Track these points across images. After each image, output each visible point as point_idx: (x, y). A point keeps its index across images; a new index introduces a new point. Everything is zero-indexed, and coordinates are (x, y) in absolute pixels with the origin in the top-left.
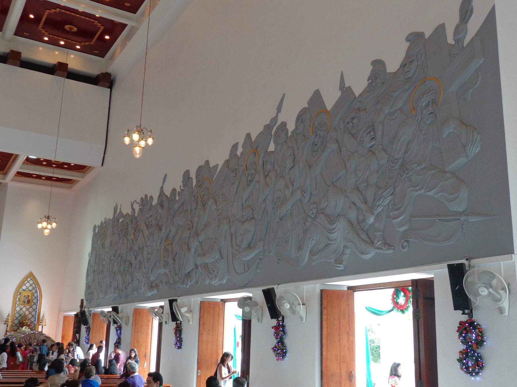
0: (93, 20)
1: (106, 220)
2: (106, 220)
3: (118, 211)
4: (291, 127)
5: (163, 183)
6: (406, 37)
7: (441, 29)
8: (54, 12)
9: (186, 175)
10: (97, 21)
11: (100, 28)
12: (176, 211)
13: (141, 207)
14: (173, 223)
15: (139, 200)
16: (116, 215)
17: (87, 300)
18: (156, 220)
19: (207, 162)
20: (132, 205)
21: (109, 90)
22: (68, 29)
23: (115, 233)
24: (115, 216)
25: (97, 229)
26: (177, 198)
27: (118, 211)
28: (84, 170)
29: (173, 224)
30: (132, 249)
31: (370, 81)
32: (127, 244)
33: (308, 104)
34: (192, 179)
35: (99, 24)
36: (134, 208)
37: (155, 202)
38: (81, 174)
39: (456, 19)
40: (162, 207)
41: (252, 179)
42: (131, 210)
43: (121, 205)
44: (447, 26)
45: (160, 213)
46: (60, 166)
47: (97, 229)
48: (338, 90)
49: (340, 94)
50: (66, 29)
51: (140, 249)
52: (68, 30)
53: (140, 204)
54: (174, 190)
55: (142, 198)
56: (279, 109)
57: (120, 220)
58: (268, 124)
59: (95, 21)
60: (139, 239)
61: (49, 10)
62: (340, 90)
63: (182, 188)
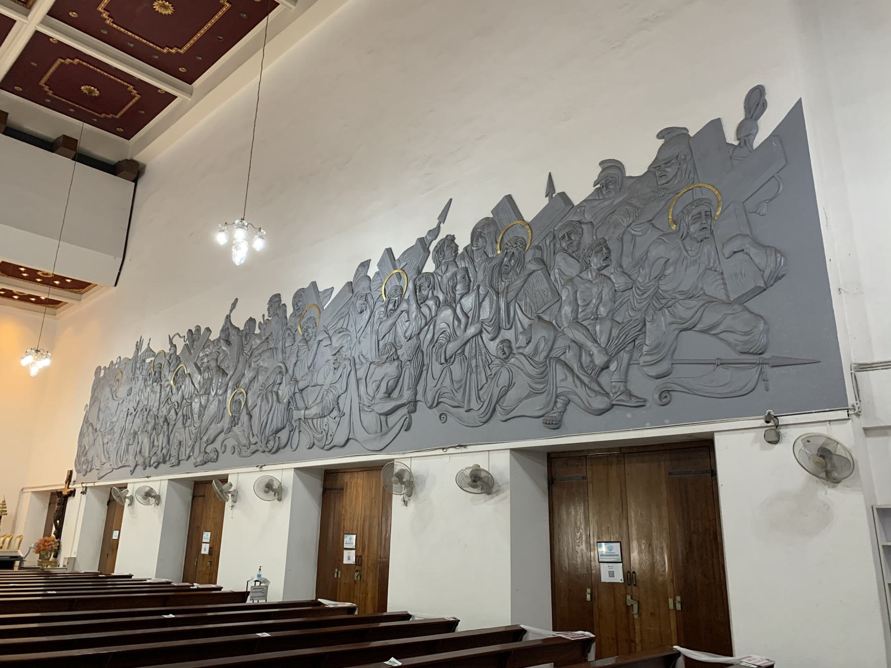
0: (126, 84)
1: (120, 360)
2: (120, 360)
3: (144, 347)
4: (463, 241)
5: (231, 311)
6: (657, 133)
7: (716, 125)
8: (70, 63)
9: (275, 301)
10: (131, 87)
11: (134, 97)
12: (254, 349)
13: (187, 342)
14: (251, 364)
15: (184, 333)
16: (139, 354)
17: (78, 472)
18: (217, 360)
19: (314, 284)
20: (171, 340)
21: (133, 184)
22: (85, 91)
23: (137, 377)
24: (138, 353)
25: (103, 371)
26: (257, 331)
27: (144, 347)
28: (84, 290)
29: (250, 367)
30: (169, 399)
31: (598, 186)
32: (161, 392)
33: (492, 213)
34: (286, 306)
35: (135, 92)
36: (174, 343)
37: (215, 335)
38: (78, 296)
39: (740, 116)
40: (228, 343)
41: (396, 307)
42: (169, 346)
43: (150, 339)
44: (724, 122)
45: (224, 351)
46: (48, 281)
47: (103, 371)
48: (544, 195)
49: (547, 202)
50: (83, 91)
51: (186, 399)
52: (86, 93)
53: (186, 338)
54: (252, 320)
55: (190, 331)
56: (443, 217)
57: (148, 361)
58: (423, 238)
59: (129, 85)
60: (183, 387)
61: (62, 59)
62: (546, 197)
63: (266, 317)
